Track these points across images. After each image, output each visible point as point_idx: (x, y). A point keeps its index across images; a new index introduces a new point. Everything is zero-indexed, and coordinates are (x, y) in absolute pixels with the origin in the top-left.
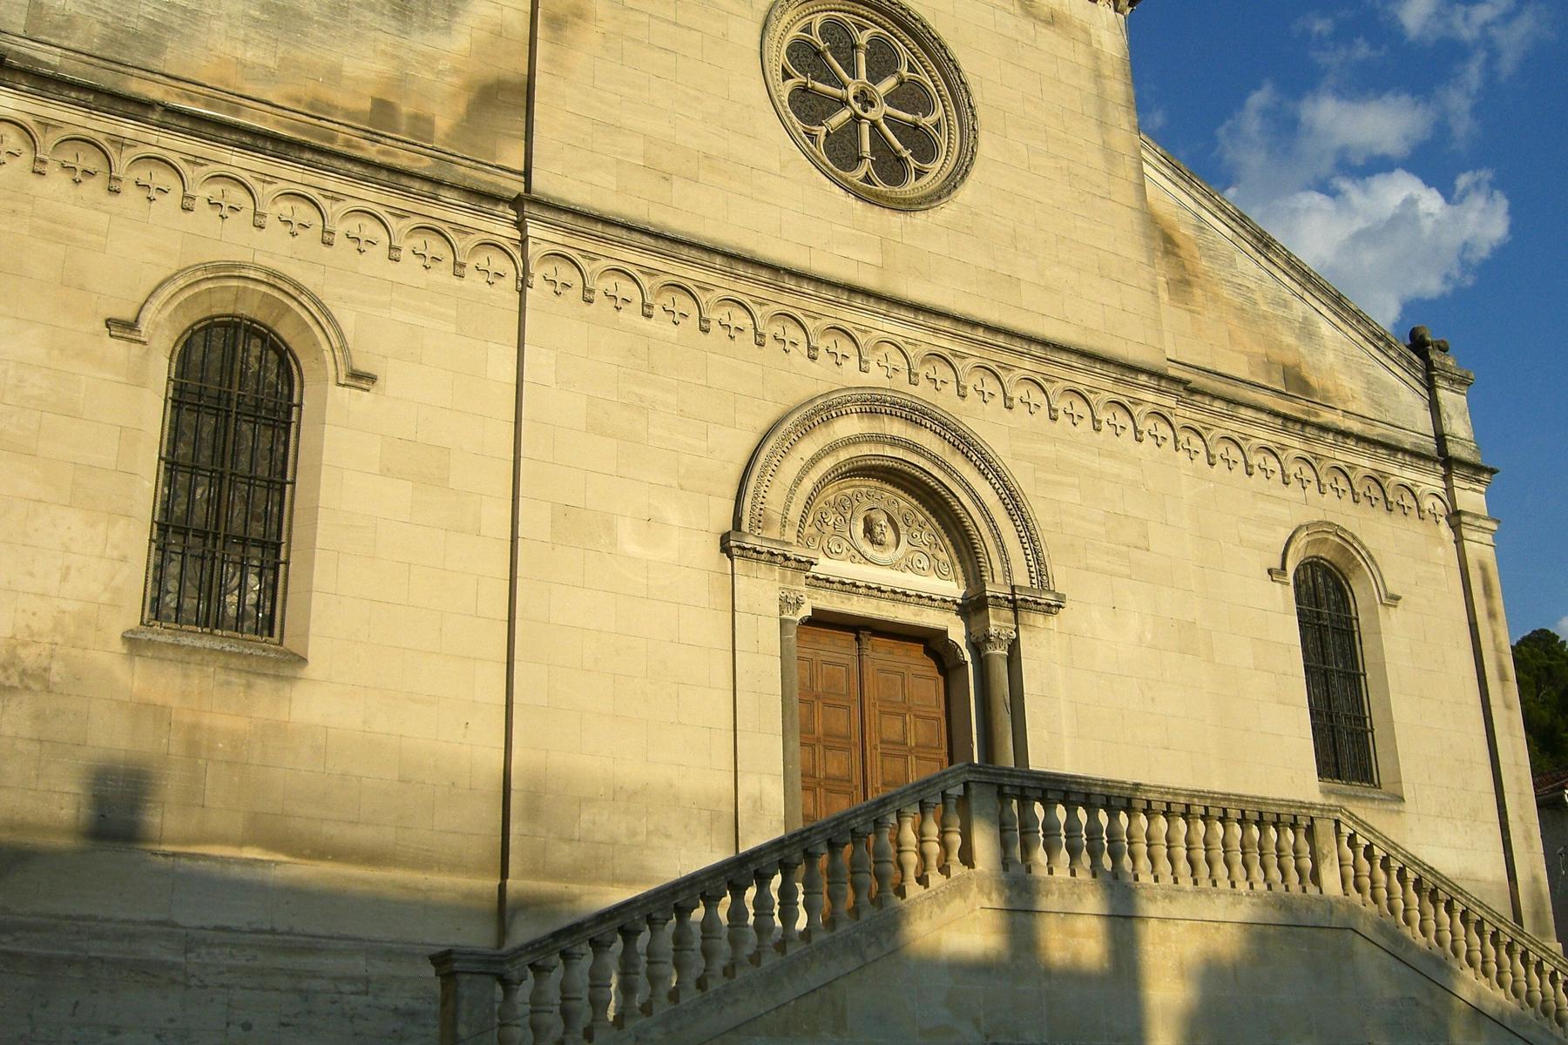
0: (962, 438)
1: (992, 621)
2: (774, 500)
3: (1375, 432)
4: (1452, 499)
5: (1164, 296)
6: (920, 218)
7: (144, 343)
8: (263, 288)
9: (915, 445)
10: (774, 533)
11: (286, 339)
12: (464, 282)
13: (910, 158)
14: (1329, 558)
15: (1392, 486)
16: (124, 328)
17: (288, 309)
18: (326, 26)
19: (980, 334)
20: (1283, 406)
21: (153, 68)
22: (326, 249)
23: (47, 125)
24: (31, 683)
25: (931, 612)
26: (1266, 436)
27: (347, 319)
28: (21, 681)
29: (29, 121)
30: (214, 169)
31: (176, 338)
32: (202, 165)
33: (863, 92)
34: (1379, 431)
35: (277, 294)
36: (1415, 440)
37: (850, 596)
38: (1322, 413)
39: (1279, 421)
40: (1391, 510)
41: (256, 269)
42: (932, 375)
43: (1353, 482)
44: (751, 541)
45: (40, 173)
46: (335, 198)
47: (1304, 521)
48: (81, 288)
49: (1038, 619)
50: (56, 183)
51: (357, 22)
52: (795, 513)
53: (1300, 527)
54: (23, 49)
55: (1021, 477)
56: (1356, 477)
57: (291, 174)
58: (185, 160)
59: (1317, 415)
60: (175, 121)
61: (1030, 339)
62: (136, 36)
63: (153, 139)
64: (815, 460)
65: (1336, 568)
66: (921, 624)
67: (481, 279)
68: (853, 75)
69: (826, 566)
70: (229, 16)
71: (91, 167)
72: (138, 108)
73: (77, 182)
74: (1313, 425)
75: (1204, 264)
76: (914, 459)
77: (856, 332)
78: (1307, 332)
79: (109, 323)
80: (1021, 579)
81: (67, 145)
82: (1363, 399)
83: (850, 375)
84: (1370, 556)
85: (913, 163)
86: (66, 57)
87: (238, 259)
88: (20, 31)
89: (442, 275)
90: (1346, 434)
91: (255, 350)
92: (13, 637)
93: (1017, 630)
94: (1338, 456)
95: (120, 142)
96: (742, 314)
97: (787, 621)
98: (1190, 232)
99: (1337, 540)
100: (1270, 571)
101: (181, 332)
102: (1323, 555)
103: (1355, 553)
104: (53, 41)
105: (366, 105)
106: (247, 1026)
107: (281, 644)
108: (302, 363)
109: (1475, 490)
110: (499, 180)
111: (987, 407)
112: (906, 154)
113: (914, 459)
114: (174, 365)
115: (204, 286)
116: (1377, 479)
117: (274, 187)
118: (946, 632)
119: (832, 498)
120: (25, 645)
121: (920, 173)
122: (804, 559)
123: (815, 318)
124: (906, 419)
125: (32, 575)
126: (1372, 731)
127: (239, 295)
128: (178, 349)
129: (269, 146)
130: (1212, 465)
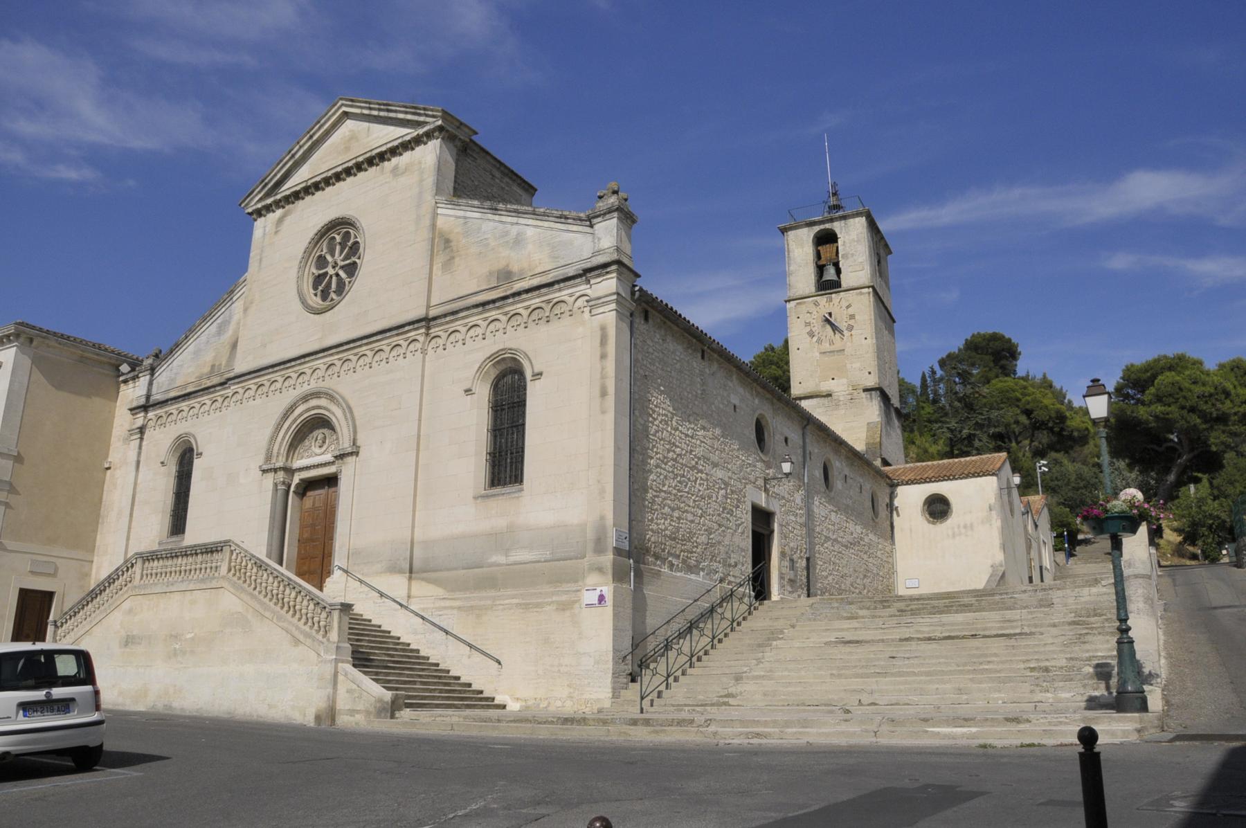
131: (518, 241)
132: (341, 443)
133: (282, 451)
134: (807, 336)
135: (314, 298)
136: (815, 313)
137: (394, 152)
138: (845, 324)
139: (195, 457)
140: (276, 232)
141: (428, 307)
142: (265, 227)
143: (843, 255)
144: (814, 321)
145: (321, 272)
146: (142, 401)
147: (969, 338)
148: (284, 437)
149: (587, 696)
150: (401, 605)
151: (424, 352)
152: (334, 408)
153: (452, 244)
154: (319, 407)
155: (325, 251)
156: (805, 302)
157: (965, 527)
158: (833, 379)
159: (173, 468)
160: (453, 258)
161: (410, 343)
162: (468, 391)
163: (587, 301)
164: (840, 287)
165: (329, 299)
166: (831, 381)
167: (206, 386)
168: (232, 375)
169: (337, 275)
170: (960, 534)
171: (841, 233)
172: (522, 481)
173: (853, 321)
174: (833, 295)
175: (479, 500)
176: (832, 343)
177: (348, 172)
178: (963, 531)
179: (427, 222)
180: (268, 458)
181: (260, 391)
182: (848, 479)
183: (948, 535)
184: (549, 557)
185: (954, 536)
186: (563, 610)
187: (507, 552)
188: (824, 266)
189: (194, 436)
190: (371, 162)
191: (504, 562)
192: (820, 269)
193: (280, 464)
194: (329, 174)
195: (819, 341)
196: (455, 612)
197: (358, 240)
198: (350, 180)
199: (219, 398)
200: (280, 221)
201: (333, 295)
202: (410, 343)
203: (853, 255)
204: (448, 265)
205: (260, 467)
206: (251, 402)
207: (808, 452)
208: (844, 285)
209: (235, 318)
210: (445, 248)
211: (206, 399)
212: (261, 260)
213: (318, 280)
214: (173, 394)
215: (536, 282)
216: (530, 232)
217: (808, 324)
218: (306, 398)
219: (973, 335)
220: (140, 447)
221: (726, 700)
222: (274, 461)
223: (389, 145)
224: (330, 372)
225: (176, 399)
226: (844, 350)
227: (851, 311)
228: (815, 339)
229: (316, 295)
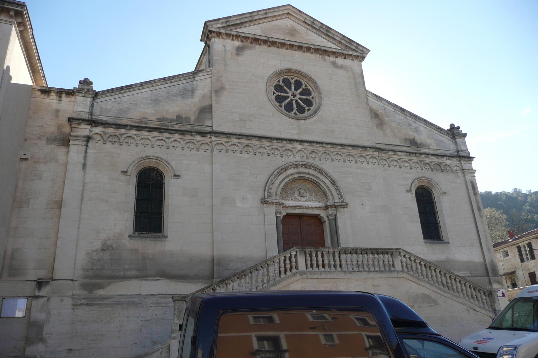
0: (320, 170)
1: (330, 211)
2: (273, 190)
3: (438, 152)
4: (462, 166)
5: (375, 128)
6: (308, 121)
7: (129, 175)
8: (154, 160)
9: (308, 173)
10: (274, 197)
11: (161, 170)
12: (199, 152)
13: (306, 107)
14: (425, 185)
15: (443, 165)
16: (125, 173)
17: (160, 164)
18: (165, 102)
19: (324, 145)
20: (410, 150)
21: (128, 117)
22: (168, 150)
23: (106, 133)
24: (109, 248)
25: (316, 210)
26: (405, 158)
27: (173, 164)
28: (107, 248)
29: (102, 133)
30: (142, 137)
31: (137, 173)
32: (140, 136)
33: (293, 94)
34: (439, 152)
35: (157, 161)
36: (450, 153)
37: (295, 209)
38: (421, 150)
39: (408, 154)
40: (443, 171)
41: (153, 156)
42: (404, 165)
43: (431, 166)
44: (267, 200)
45: (105, 143)
46: (169, 139)
47: (416, 177)
48: (116, 166)
49: (342, 209)
50: (109, 145)
51: (172, 100)
52: (279, 192)
53: (415, 179)
54: (99, 118)
55: (336, 177)
56: (432, 165)
57: (159, 135)
58: (136, 136)
59: (420, 151)
60: (133, 128)
61: (337, 145)
62: (124, 111)
63: (129, 133)
64: (283, 180)
65: (428, 187)
66: (314, 213)
67: (203, 151)
68: (290, 89)
69: (287, 203)
70: (144, 104)
71: (115, 140)
72: (124, 127)
73: (113, 144)
74: (418, 153)
75: (386, 118)
76: (308, 176)
77: (292, 149)
78: (417, 131)
79: (122, 172)
80: (337, 200)
81: (110, 137)
82: (434, 145)
83: (292, 159)
84: (437, 184)
85: (307, 108)
86: (109, 118)
87: (148, 155)
88: (99, 115)
89: (194, 152)
90: (428, 154)
91: (155, 173)
92: (105, 239)
93: (336, 212)
94: (426, 160)
95: (121, 134)
96: (264, 149)
97: (278, 217)
98: (382, 112)
99: (427, 181)
100: (407, 191)
101: (138, 172)
102: (423, 185)
103: (432, 183)
104: (106, 115)
105: (175, 117)
106: (156, 315)
107: (163, 234)
108: (165, 174)
109: (468, 163)
110: (204, 129)
111: (327, 162)
112: (305, 106)
113: (308, 176)
114: (137, 179)
115: (141, 162)
116: (439, 164)
117: (155, 138)
118: (320, 215)
119: (290, 188)
120: (108, 240)
121: (308, 110)
122: (281, 202)
123: (282, 148)
124: (306, 167)
125: (108, 226)
126: (440, 226)
127: (149, 162)
128: (138, 175)
129: (153, 130)
130: (389, 167)
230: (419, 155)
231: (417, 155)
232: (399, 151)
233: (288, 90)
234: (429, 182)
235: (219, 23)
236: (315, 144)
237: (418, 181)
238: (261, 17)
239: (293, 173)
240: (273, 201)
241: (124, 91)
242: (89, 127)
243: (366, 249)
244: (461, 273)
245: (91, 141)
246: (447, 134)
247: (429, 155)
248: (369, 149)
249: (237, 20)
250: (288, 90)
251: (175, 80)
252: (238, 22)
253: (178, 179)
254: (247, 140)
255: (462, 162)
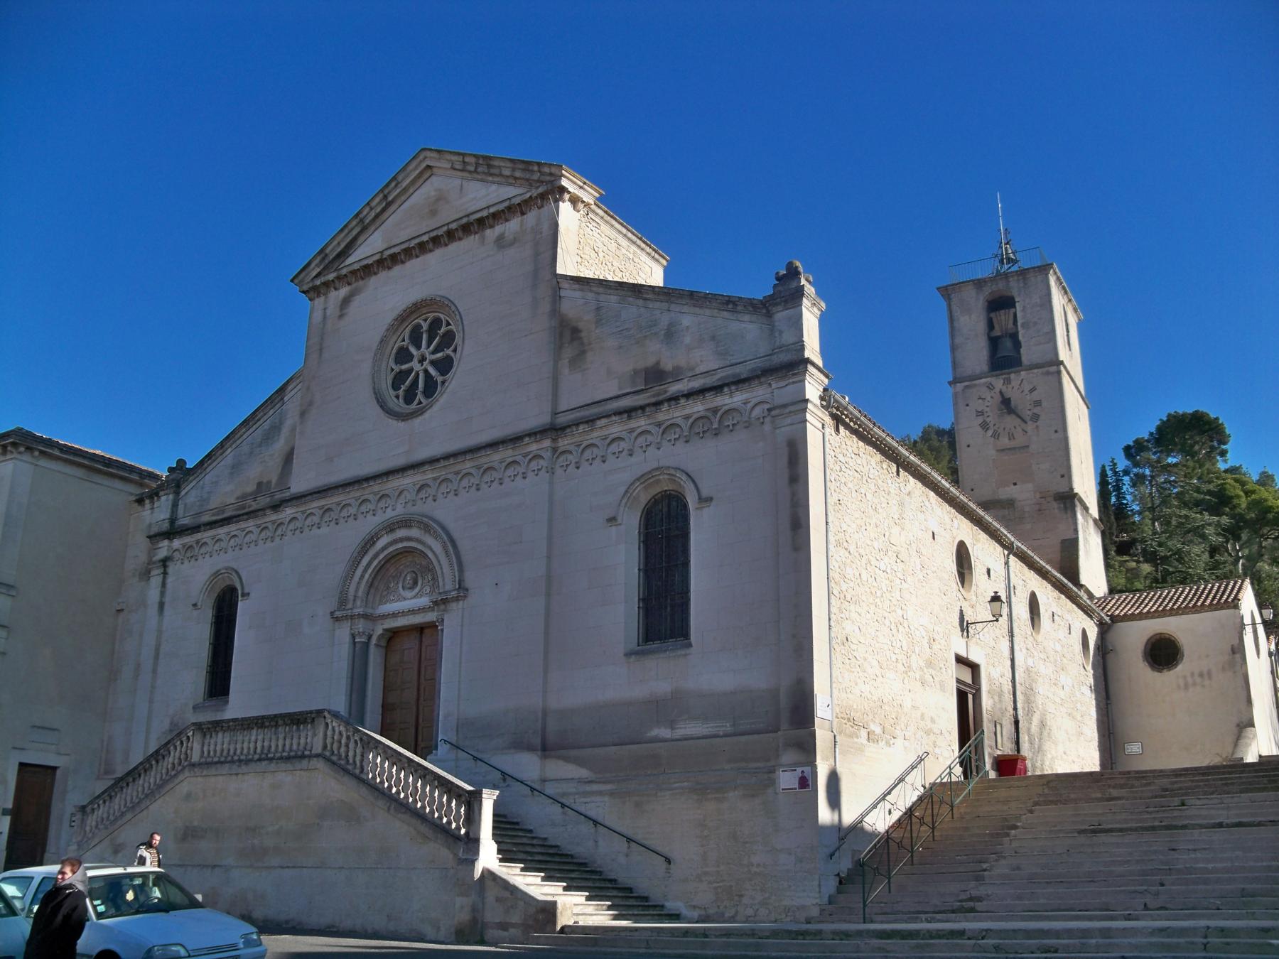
19: (443, 463)
39: (626, 415)
99: (666, 477)
109: (794, 383)
131: (670, 335)
132: (441, 584)
133: (360, 594)
134: (981, 429)
135: (395, 400)
136: (989, 398)
137: (497, 217)
138: (1028, 412)
139: (240, 598)
140: (341, 316)
141: (555, 414)
142: (325, 309)
143: (1023, 325)
144: (988, 409)
145: (404, 367)
146: (166, 526)
147: (1165, 419)
148: (362, 576)
149: (786, 903)
150: (532, 789)
151: (551, 471)
152: (429, 540)
153: (583, 334)
154: (409, 539)
155: (407, 341)
156: (975, 385)
157: (1201, 675)
158: (1015, 484)
159: (208, 614)
160: (583, 352)
161: (530, 460)
162: (612, 520)
163: (769, 410)
164: (1021, 366)
165: (416, 402)
166: (1012, 486)
167: (251, 509)
168: (287, 494)
169: (426, 371)
170: (1194, 684)
171: (1019, 295)
172: (686, 635)
173: (1039, 408)
174: (1013, 376)
175: (633, 658)
176: (1011, 437)
177: (436, 241)
178: (1198, 680)
179: (546, 307)
180: (343, 602)
181: (326, 518)
182: (1056, 617)
183: (1179, 687)
184: (729, 729)
185: (1186, 687)
186: (753, 796)
187: (672, 725)
188: (998, 338)
189: (237, 572)
190: (467, 229)
191: (669, 736)
192: (994, 342)
193: (359, 610)
194: (413, 243)
195: (996, 435)
196: (606, 799)
197: (452, 327)
198: (439, 252)
199: (269, 525)
200: (346, 301)
201: (420, 397)
202: (530, 460)
203: (1035, 323)
204: (578, 360)
205: (332, 613)
206: (315, 531)
207: (1012, 585)
208: (1025, 359)
209: (288, 423)
210: (573, 340)
211: (250, 524)
212: (321, 350)
213: (399, 379)
214: (206, 518)
215: (696, 384)
216: (686, 321)
217: (980, 413)
218: (391, 527)
219: (1169, 415)
220: (164, 584)
221: (971, 904)
222: (350, 606)
223: (492, 210)
224: (422, 495)
225: (212, 525)
226: (1027, 447)
227: (1035, 396)
228: (990, 433)
229: (397, 397)
230: (653, 408)
231: (648, 409)
232: (600, 418)
233: (432, 347)
234: (672, 479)
235: (313, 269)
236: (426, 468)
237: (642, 486)
238: (378, 210)
239: (385, 546)
240: (349, 613)
241: (206, 465)
242: (166, 542)
243: (275, 716)
244: (707, 728)
245: (168, 563)
246: (753, 307)
247: (679, 400)
248: (527, 439)
249: (339, 244)
250: (432, 347)
251: (259, 416)
252: (343, 246)
253: (247, 601)
254: (328, 499)
255: (774, 386)
